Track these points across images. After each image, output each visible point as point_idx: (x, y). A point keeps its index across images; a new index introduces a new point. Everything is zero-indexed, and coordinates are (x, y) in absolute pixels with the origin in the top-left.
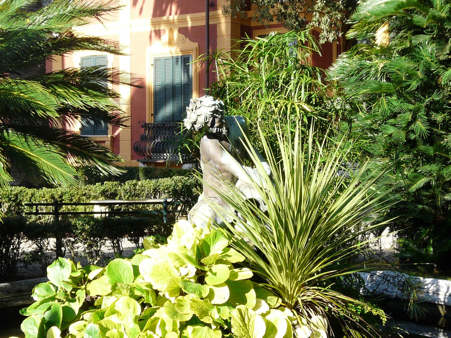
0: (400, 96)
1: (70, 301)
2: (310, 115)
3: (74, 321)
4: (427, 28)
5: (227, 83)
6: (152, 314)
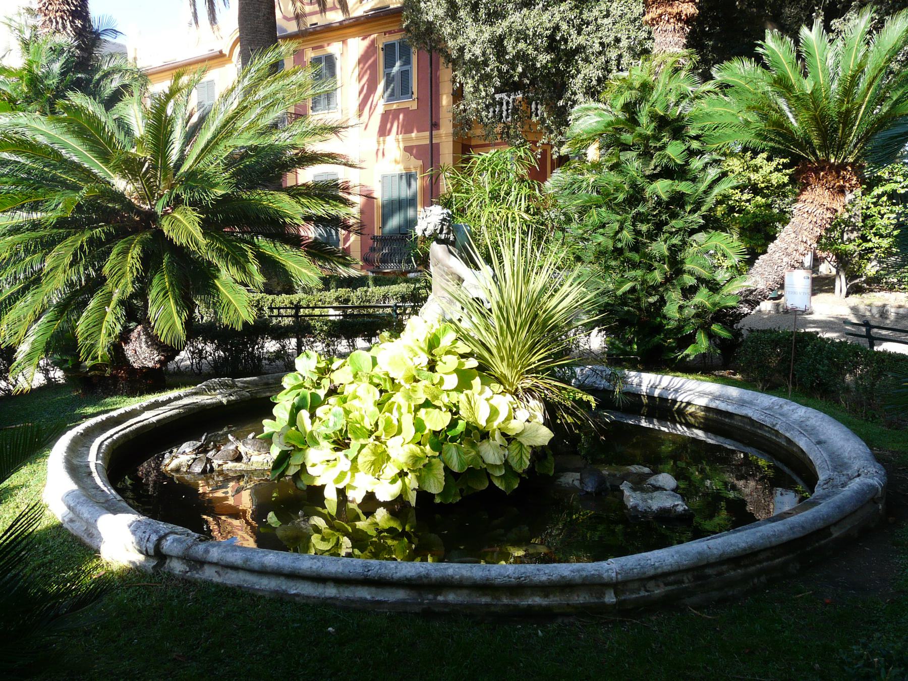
0: (609, 207)
1: (316, 388)
2: (528, 223)
3: (319, 406)
4: (634, 145)
5: (454, 195)
6: (389, 398)
